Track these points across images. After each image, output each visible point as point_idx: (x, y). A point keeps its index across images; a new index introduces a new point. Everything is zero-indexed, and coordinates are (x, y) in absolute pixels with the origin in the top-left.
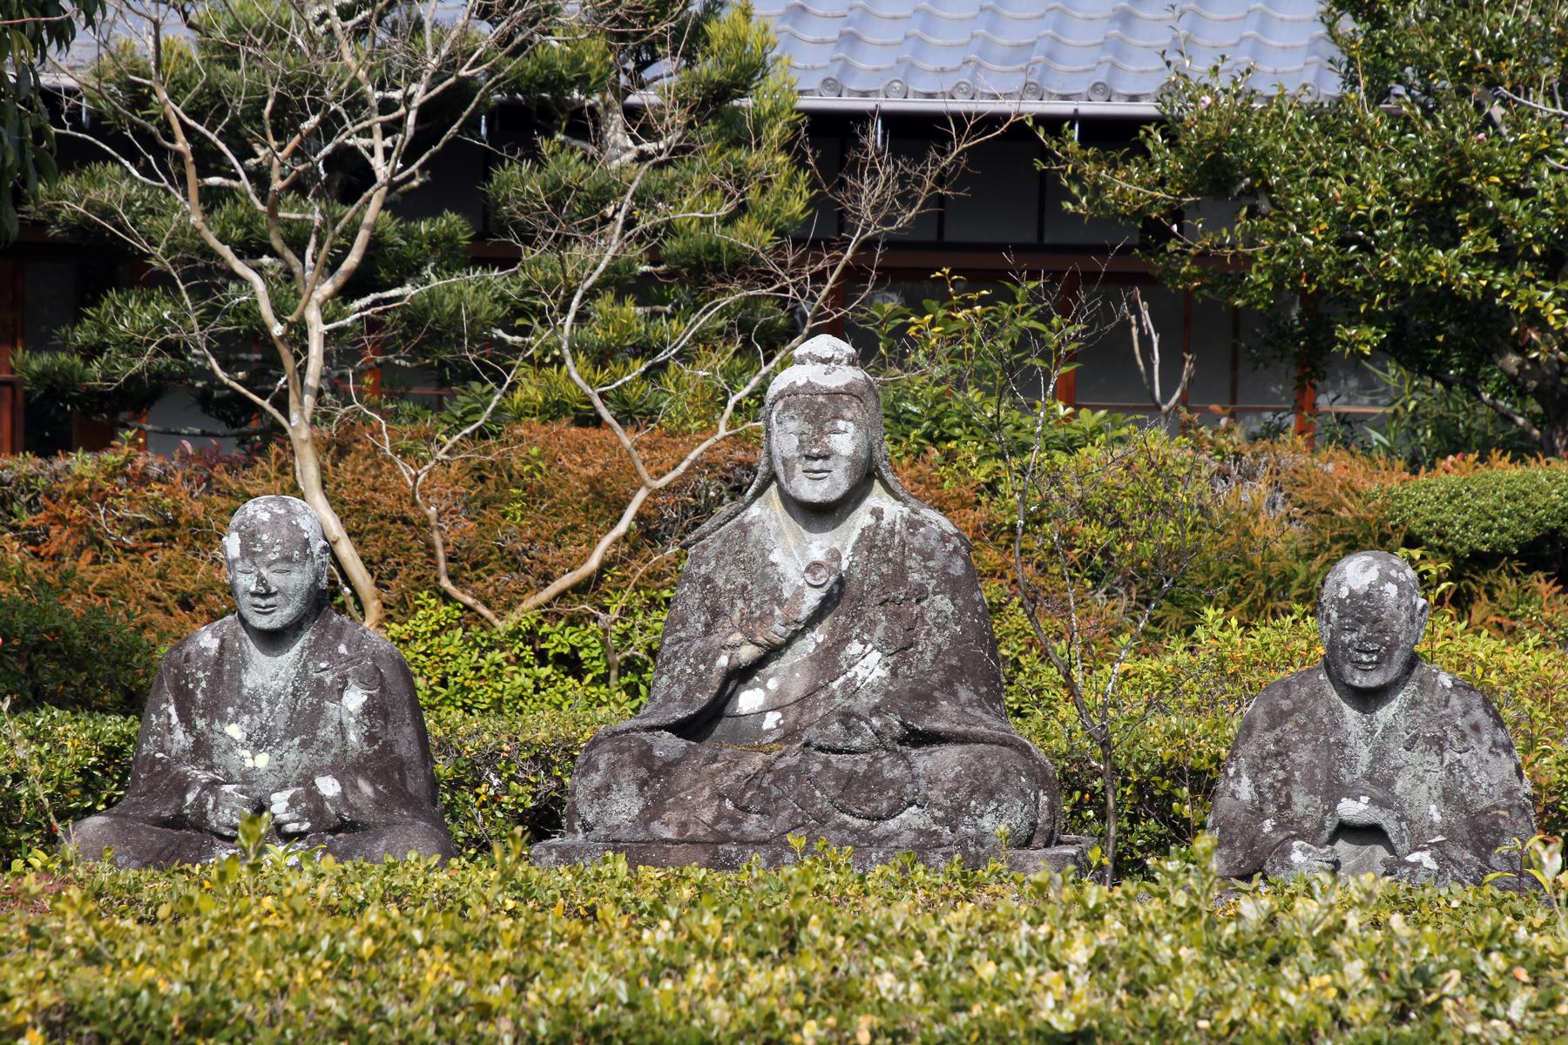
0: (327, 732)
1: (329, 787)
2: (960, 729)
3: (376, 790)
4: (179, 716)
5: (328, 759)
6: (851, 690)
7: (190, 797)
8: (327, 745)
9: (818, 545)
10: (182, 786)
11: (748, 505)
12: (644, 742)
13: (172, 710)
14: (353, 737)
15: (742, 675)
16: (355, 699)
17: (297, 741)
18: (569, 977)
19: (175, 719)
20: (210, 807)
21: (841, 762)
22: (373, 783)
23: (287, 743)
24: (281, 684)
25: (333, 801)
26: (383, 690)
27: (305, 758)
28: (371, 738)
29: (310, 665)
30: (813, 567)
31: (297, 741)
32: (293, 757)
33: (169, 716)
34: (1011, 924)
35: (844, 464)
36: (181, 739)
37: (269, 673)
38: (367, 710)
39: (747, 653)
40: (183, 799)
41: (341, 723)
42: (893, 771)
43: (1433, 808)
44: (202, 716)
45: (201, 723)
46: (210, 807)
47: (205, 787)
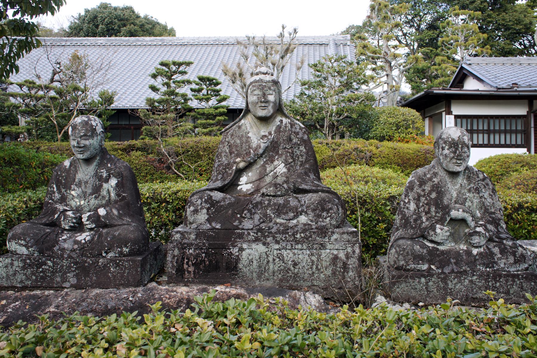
0: (104, 193)
1: (102, 212)
2: (314, 188)
3: (119, 213)
4: (57, 188)
5: (104, 202)
6: (276, 177)
7: (56, 216)
8: (104, 197)
9: (264, 131)
10: (55, 211)
11: (240, 120)
12: (209, 195)
13: (55, 186)
14: (113, 195)
15: (240, 172)
16: (113, 182)
17: (94, 196)
18: (383, 305)
19: (55, 190)
20: (62, 219)
21: (274, 200)
22: (118, 211)
23: (91, 197)
24: (89, 177)
25: (103, 217)
26: (122, 180)
27: (97, 202)
28: (118, 195)
29: (98, 171)
30: (263, 137)
31: (94, 196)
32: (93, 202)
33: (54, 188)
34: (286, 348)
35: (272, 104)
36: (57, 196)
37: (85, 173)
38: (117, 185)
39: (242, 165)
40: (54, 217)
41: (108, 190)
42: (293, 202)
43: (478, 212)
44: (64, 188)
45: (63, 190)
46: (62, 219)
47: (61, 212)
